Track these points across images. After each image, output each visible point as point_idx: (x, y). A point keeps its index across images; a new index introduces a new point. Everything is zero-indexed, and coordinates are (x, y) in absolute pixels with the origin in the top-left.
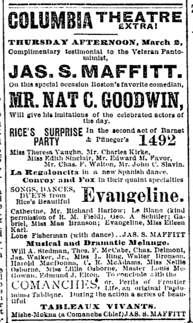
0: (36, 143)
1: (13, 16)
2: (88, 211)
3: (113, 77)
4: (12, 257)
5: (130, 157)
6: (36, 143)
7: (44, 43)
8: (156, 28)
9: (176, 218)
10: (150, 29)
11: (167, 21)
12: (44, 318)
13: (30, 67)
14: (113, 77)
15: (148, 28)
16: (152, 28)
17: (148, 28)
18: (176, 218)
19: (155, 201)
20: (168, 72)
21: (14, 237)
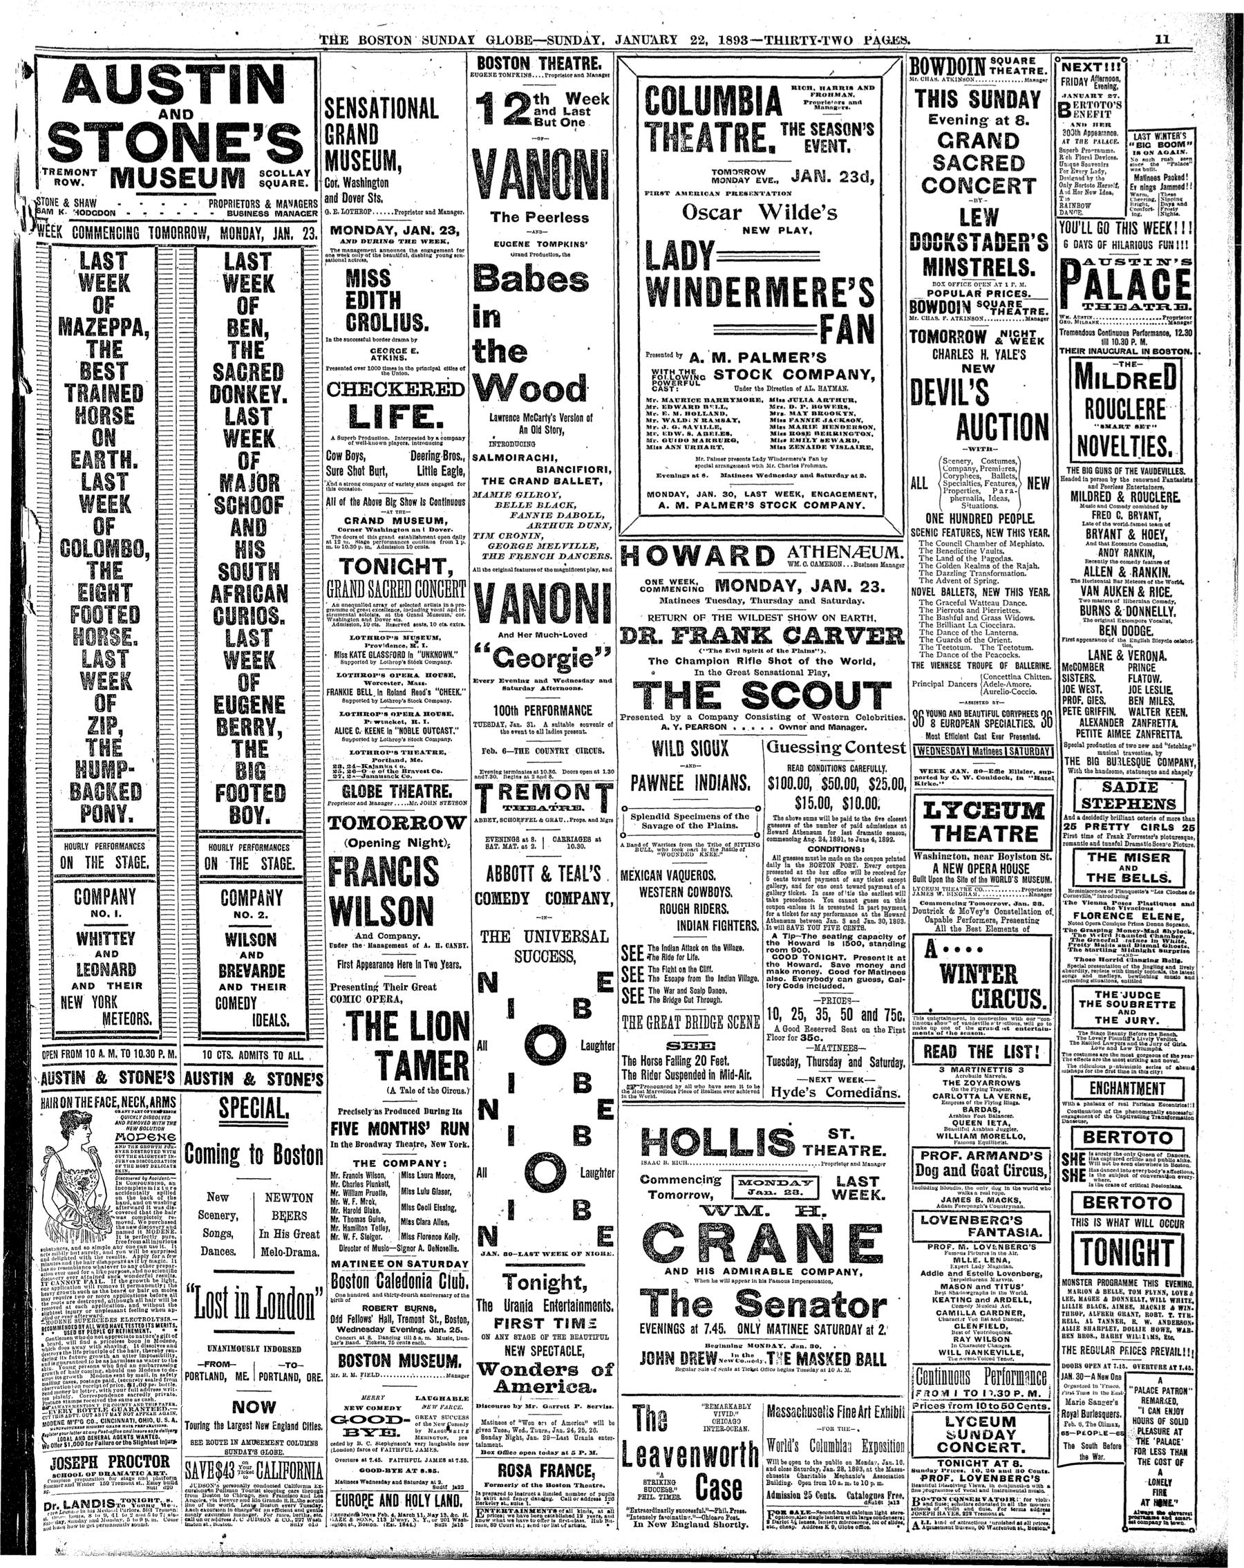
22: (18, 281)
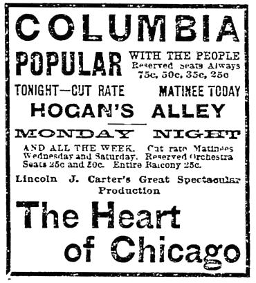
0: (22, 68)
1: (74, 87)
2: (118, 157)
3: (94, 116)
4: (72, 178)
5: (101, 106)
6: (22, 68)
8: (237, 95)
9: (143, 181)
10: (88, 117)
11: (186, 87)
12: (168, 266)
13: (92, 106)
14: (94, 116)
15: (84, 116)
16: (163, 116)
17: (84, 116)
18: (143, 181)
19: (72, 53)
20: (90, 30)
21: (229, 58)
22: (143, 275)
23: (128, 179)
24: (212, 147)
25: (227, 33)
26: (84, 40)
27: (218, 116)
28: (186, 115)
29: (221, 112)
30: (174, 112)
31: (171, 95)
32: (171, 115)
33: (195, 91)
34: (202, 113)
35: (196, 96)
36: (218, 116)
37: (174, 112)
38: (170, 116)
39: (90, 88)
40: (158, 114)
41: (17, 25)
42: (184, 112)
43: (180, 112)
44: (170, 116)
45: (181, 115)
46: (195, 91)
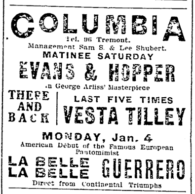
7: (75, 57)
10: (23, 177)
15: (20, 176)
23: (160, 186)
24: (168, 27)
25: (173, 34)
26: (86, 15)
27: (150, 59)
28: (157, 123)
29: (86, 71)
30: (74, 175)
31: (107, 58)
32: (146, 123)
33: (160, 73)
34: (84, 176)
35: (162, 80)
36: (150, 59)
37: (74, 175)
38: (71, 177)
39: (144, 99)
40: (23, 164)
41: (84, 30)
42: (71, 174)
43: (153, 120)
44: (71, 177)
45: (154, 123)
46: (160, 73)
